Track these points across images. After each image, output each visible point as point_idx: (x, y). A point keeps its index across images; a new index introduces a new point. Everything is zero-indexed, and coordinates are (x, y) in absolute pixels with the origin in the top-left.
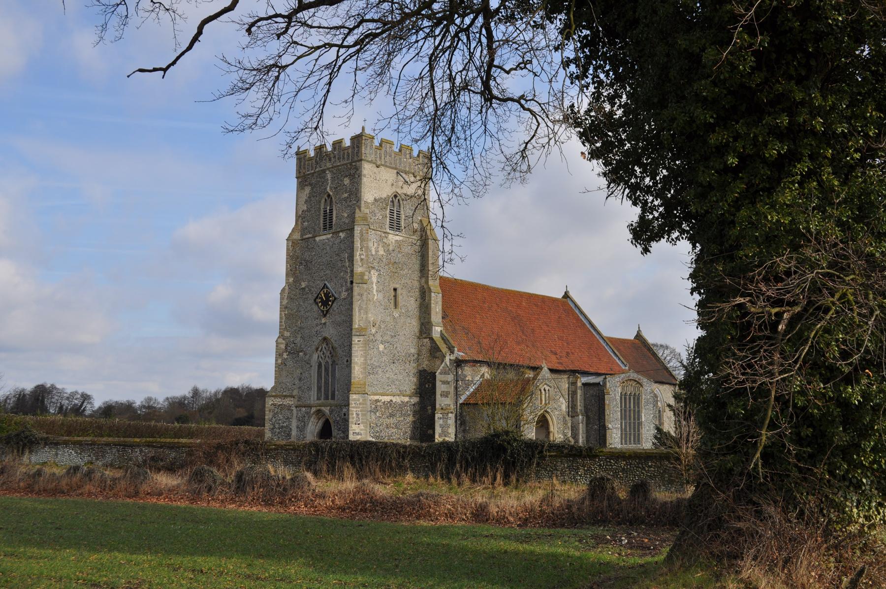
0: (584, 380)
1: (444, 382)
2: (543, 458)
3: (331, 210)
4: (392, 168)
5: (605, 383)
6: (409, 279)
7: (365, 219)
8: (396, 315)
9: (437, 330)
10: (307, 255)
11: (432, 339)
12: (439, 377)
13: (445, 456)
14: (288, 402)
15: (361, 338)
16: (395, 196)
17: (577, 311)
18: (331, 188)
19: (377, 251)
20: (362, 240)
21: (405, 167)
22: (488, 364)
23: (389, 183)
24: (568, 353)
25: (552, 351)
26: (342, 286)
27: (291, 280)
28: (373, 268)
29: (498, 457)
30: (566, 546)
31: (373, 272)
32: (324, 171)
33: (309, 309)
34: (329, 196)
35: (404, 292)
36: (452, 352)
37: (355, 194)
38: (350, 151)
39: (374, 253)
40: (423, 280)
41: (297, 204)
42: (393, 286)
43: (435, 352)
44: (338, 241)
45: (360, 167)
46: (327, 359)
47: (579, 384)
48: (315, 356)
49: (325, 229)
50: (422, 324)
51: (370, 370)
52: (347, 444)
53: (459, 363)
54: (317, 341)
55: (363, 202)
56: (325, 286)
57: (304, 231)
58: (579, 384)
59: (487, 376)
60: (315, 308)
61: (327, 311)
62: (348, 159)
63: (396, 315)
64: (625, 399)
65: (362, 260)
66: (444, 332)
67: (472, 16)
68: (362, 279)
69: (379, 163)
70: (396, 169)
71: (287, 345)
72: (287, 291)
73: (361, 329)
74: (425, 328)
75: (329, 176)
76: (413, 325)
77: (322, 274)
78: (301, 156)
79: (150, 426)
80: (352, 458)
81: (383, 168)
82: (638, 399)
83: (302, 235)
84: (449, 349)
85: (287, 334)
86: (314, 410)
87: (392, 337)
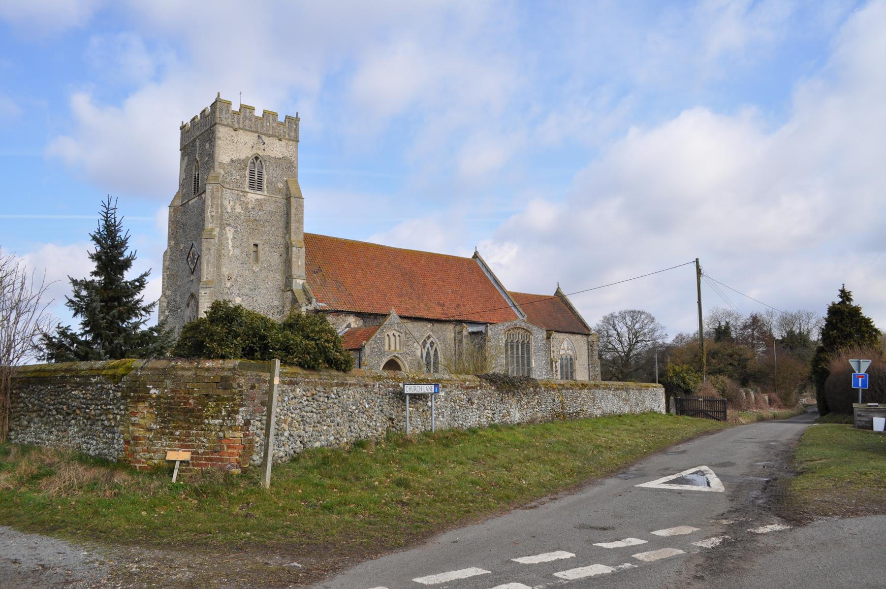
0: (471, 329)
4: (253, 132)
5: (487, 331)
6: (271, 234)
9: (298, 283)
15: (208, 291)
16: (257, 158)
17: (484, 270)
19: (233, 209)
20: (213, 198)
21: (268, 131)
22: (358, 314)
23: (249, 145)
25: (439, 304)
27: (172, 243)
28: (229, 225)
30: (668, 487)
31: (227, 229)
35: (267, 248)
39: (229, 210)
42: (252, 242)
47: (465, 333)
55: (216, 163)
58: (465, 333)
64: (517, 346)
65: (212, 216)
66: (307, 286)
68: (210, 235)
69: (236, 126)
70: (257, 132)
71: (168, 303)
72: (169, 254)
73: (208, 282)
76: (278, 278)
81: (242, 131)
82: (528, 346)
84: (308, 300)
85: (168, 293)
87: (251, 290)
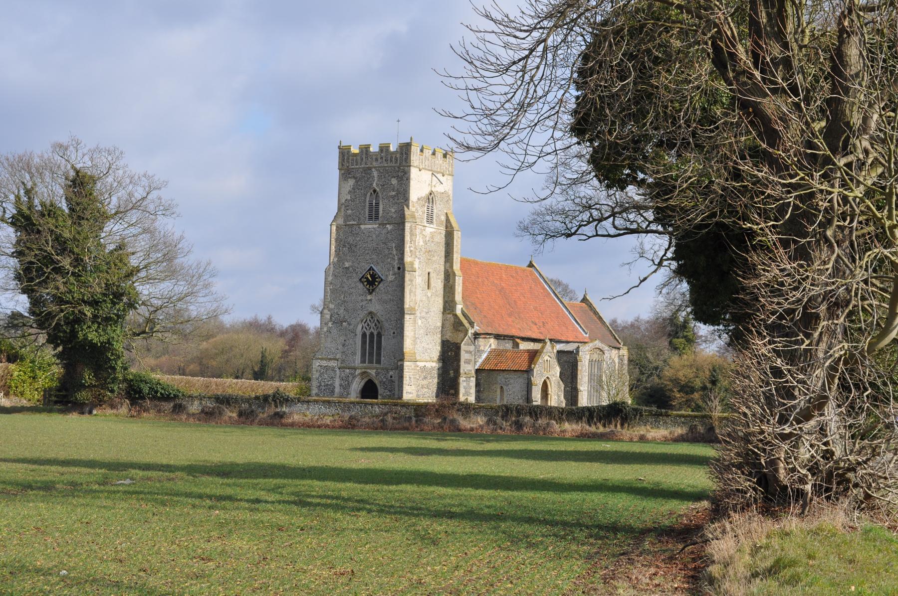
0: (560, 347)
1: (467, 352)
2: (641, 416)
3: (377, 204)
7: (413, 217)
8: (429, 294)
10: (350, 239)
11: (456, 315)
12: (463, 347)
13: (587, 414)
14: (333, 364)
15: (412, 317)
18: (377, 185)
24: (543, 323)
26: (389, 270)
29: (618, 415)
32: (370, 169)
33: (353, 285)
34: (375, 191)
36: (473, 327)
37: (403, 195)
38: (398, 156)
40: (448, 265)
41: (339, 193)
43: (458, 325)
44: (384, 231)
45: (409, 171)
46: (372, 330)
48: (360, 327)
49: (370, 218)
50: (445, 302)
51: (415, 339)
52: (578, 409)
53: (476, 335)
54: (362, 314)
56: (371, 269)
57: (347, 218)
59: (493, 347)
60: (360, 286)
61: (373, 290)
62: (396, 162)
63: (429, 294)
67: (660, 228)
68: (412, 267)
71: (331, 316)
74: (449, 305)
75: (375, 174)
77: (368, 257)
78: (344, 153)
79: (658, 407)
80: (530, 413)
83: (345, 221)
85: (332, 306)
86: (358, 372)
